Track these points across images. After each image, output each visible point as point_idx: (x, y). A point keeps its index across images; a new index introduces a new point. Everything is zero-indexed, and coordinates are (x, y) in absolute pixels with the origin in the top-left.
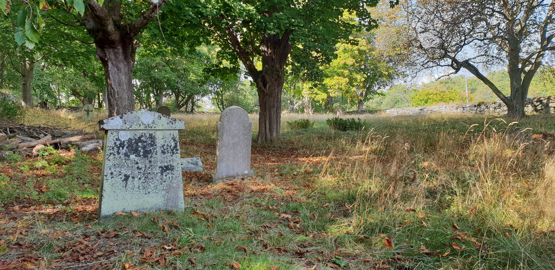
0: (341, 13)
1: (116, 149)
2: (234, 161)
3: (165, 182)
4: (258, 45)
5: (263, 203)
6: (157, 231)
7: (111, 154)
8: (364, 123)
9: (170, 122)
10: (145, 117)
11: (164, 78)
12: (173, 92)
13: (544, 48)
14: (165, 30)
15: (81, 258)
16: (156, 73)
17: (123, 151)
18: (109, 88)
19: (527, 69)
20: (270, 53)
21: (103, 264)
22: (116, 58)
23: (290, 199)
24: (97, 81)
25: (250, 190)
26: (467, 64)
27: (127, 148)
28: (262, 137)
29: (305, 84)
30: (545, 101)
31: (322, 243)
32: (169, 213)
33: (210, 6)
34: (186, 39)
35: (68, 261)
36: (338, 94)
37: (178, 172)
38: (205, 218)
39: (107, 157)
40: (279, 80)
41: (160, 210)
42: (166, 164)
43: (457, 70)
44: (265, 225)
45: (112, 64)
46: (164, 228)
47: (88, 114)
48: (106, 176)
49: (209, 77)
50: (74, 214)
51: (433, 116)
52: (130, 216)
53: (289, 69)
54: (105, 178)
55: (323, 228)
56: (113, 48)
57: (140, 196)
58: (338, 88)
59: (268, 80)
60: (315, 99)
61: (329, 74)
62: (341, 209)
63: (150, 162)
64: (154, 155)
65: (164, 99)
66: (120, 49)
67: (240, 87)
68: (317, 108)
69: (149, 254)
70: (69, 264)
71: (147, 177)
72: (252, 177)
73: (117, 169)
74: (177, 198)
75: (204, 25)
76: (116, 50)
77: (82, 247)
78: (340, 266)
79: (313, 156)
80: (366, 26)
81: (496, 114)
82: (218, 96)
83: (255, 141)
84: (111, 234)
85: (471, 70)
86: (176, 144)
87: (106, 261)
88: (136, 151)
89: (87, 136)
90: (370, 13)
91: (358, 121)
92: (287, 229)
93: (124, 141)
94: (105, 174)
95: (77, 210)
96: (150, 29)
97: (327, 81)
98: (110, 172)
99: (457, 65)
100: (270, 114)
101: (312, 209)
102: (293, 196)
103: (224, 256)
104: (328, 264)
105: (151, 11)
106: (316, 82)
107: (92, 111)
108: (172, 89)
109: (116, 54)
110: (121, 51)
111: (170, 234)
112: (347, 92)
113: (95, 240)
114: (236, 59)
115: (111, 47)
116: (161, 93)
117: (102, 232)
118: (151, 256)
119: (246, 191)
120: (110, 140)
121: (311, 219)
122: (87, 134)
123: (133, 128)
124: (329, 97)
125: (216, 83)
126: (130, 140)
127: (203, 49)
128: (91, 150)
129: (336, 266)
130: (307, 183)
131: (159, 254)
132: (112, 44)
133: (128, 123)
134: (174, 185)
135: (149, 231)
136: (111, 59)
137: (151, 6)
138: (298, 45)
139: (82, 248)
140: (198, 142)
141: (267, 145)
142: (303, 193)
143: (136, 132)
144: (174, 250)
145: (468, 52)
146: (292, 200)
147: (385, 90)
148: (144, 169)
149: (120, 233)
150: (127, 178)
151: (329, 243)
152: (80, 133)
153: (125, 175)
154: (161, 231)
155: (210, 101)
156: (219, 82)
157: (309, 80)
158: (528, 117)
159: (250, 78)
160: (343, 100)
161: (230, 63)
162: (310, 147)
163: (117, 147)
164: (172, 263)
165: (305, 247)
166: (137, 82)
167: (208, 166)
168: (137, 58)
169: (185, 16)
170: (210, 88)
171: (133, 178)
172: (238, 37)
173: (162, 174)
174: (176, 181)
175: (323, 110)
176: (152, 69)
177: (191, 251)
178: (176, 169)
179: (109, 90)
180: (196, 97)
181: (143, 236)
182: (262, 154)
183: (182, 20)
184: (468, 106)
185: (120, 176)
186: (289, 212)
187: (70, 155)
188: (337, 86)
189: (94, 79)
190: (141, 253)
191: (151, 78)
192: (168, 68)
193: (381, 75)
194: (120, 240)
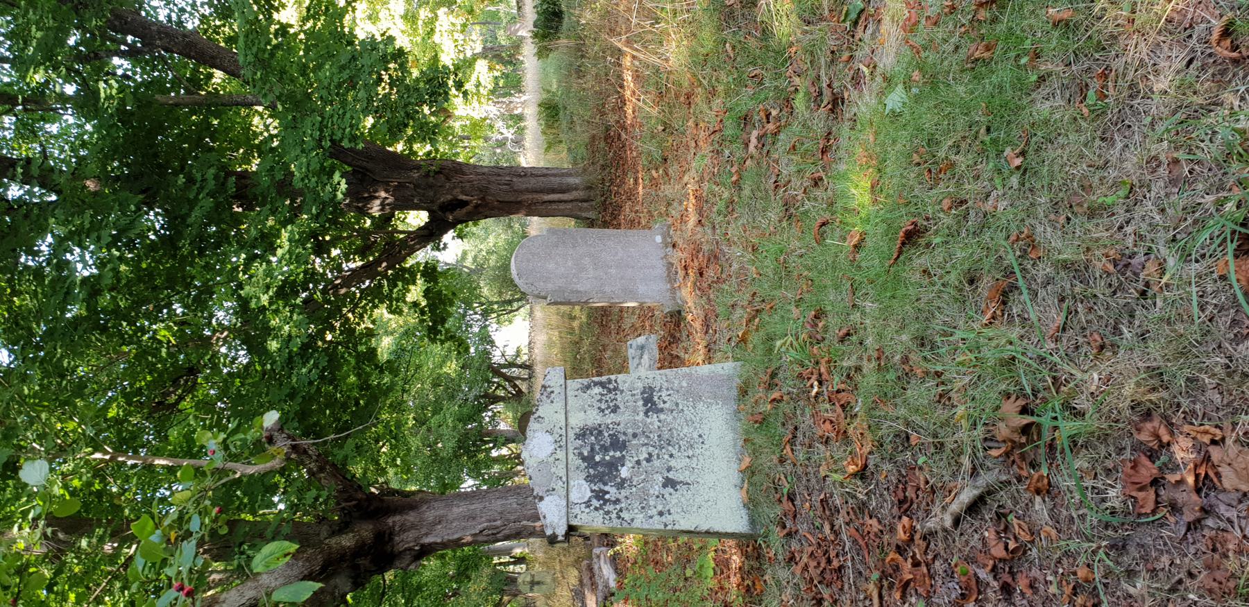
0: (283, 29)
1: (608, 507)
2: (633, 266)
3: (677, 404)
4: (369, 222)
5: (726, 195)
6: (781, 414)
10: (539, 447)
11: (455, 428)
12: (486, 409)
14: (346, 427)
15: (835, 564)
16: (445, 446)
17: (612, 492)
18: (480, 538)
20: (387, 191)
21: (847, 520)
22: (413, 526)
23: (718, 135)
24: (467, 569)
25: (699, 229)
27: (605, 484)
28: (580, 209)
29: (457, 113)
31: (812, 53)
32: (743, 392)
33: (287, 328)
34: (366, 381)
35: (842, 589)
36: (476, 33)
37: (659, 378)
38: (754, 317)
40: (450, 170)
41: (738, 412)
42: (641, 403)
44: (773, 186)
45: (427, 535)
46: (774, 400)
47: (538, 583)
48: (666, 525)
49: (447, 331)
50: (748, 591)
52: (750, 473)
53: (421, 149)
54: (669, 527)
55: (781, 56)
57: (708, 453)
58: (462, 32)
59: (449, 197)
60: (490, 87)
61: (428, 56)
62: (738, 13)
63: (635, 435)
65: (503, 426)
66: (394, 520)
67: (469, 262)
68: (510, 85)
69: (828, 426)
70: (846, 587)
72: (669, 227)
73: (652, 503)
75: (331, 342)
76: (397, 528)
77: (813, 564)
78: (862, 11)
79: (622, 87)
82: (493, 311)
83: (591, 224)
84: (787, 508)
86: (596, 384)
87: (843, 512)
88: (614, 466)
89: (586, 580)
92: (782, 136)
93: (592, 491)
94: (662, 527)
95: (738, 586)
96: (346, 457)
97: (447, 58)
98: (657, 518)
100: (528, 191)
101: (740, 82)
102: (712, 130)
103: (834, 268)
104: (857, 37)
105: (303, 457)
106: (451, 83)
107: (533, 576)
108: (480, 411)
109: (404, 529)
110: (397, 518)
111: (787, 386)
112: (471, 12)
113: (800, 541)
114: (404, 270)
115: (391, 539)
116: (489, 434)
117: (784, 527)
118: (832, 422)
119: (699, 236)
120: (592, 521)
121: (761, 83)
122: (581, 581)
123: (562, 473)
124: (483, 55)
125: (464, 316)
126: (589, 479)
127: (385, 346)
128: (616, 570)
129: (863, 18)
130: (682, 99)
131: (828, 406)
133: (553, 485)
134: (684, 384)
135: (781, 429)
136: (416, 539)
137: (293, 456)
138: (364, 127)
139: (815, 564)
140: (596, 340)
141: (596, 195)
142: (705, 107)
143: (571, 467)
144: (820, 375)
146: (720, 130)
148: (651, 449)
149: (785, 491)
150: (669, 483)
151: (811, 37)
153: (665, 486)
154: (781, 405)
155: (504, 328)
156: (461, 311)
157: (447, 100)
159: (448, 237)
160: (491, 21)
161: (414, 283)
162: (602, 96)
163: (605, 504)
164: (848, 376)
165: (820, 94)
166: (468, 484)
167: (647, 324)
168: (413, 488)
169: (311, 383)
170: (476, 330)
171: (669, 469)
172: (352, 265)
173: (662, 410)
174: (676, 382)
175: (514, 71)
176: (437, 454)
177: (824, 339)
180: (497, 358)
181: (792, 441)
182: (620, 207)
183: (319, 389)
186: (745, 136)
188: (456, 35)
189: (463, 574)
190: (827, 442)
191: (456, 457)
192: (433, 422)
194: (801, 490)
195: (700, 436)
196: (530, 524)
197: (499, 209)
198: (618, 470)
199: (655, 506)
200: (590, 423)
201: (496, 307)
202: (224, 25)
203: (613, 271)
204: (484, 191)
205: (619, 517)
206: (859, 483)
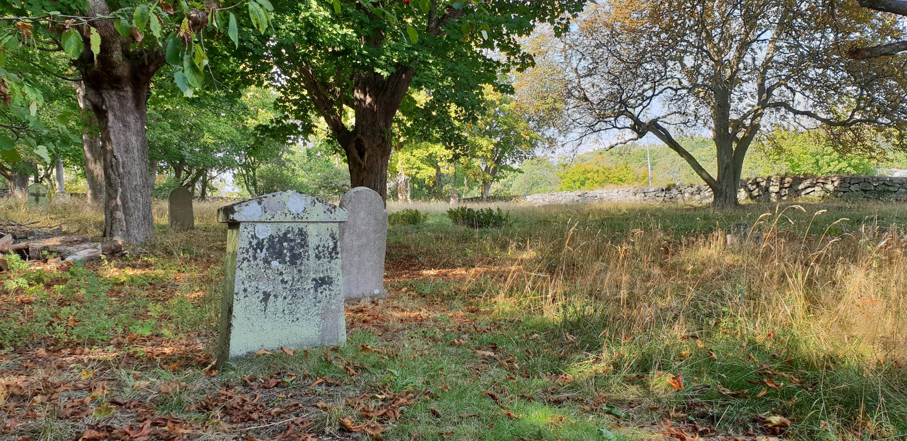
3: (320, 302)
7: (244, 259)
8: (507, 215)
9: (328, 210)
11: (160, 139)
13: (763, 104)
17: (261, 255)
18: (109, 156)
19: (740, 135)
26: (654, 126)
29: (400, 153)
30: (764, 184)
40: (384, 149)
42: (322, 276)
43: (641, 135)
45: (115, 115)
47: (37, 200)
48: (237, 294)
51: (605, 206)
54: (235, 296)
56: (118, 89)
63: (300, 271)
64: (305, 261)
66: (129, 91)
73: (253, 283)
76: (122, 93)
80: (517, 64)
81: (695, 204)
85: (660, 136)
86: (335, 243)
88: (280, 256)
89: (69, 239)
90: (519, 46)
93: (263, 240)
98: (242, 287)
99: (640, 129)
110: (130, 94)
114: (306, 111)
115: (113, 88)
123: (276, 219)
124: (439, 175)
126: (271, 238)
132: (115, 83)
136: (112, 108)
143: (280, 225)
145: (656, 109)
147: (526, 166)
150: (267, 296)
152: (59, 232)
153: (264, 293)
158: (743, 207)
163: (254, 249)
171: (276, 296)
173: (316, 291)
178: (336, 282)
179: (108, 160)
184: (651, 190)
185: (257, 295)
187: (52, 266)
195: (298, 319)
196: (119, 194)
198: (276, 259)
199: (251, 286)
203: (356, 259)
205: (244, 259)
206: (337, 428)
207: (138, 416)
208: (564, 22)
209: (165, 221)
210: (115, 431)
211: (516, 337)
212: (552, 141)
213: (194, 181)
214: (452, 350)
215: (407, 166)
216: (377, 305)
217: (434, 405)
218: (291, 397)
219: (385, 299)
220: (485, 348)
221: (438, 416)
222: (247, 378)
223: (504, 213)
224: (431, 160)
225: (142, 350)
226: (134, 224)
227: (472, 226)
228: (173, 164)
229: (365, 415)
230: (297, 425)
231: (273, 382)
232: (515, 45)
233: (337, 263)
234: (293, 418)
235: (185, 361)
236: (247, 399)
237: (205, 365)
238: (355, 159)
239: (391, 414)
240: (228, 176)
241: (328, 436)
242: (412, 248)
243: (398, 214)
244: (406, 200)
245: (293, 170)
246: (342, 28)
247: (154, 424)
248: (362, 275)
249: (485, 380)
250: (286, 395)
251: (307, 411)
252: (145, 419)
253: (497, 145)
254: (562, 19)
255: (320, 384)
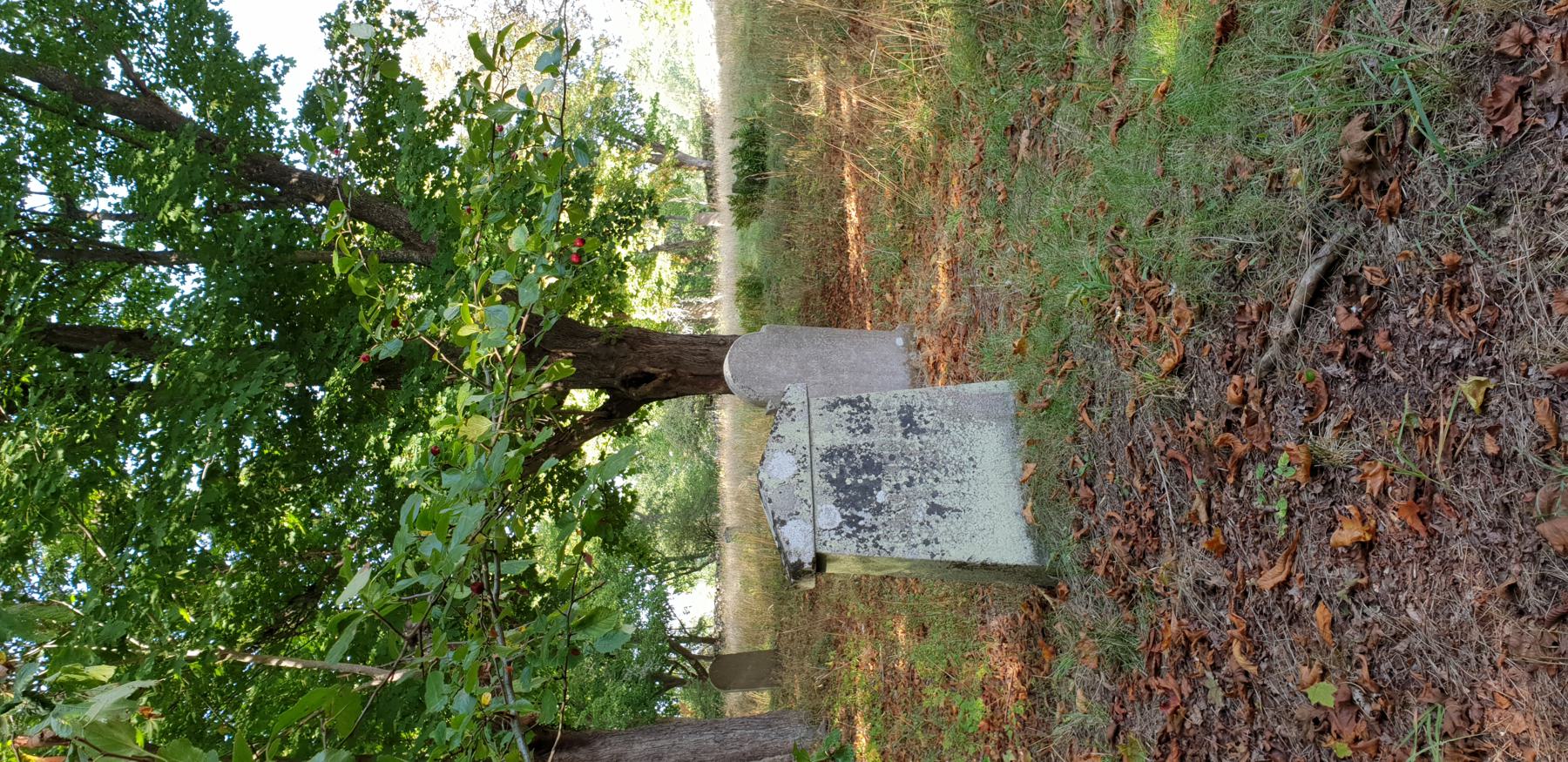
3: (942, 425)
7: (876, 546)
9: (788, 415)
17: (867, 518)
27: (859, 509)
39: (883, 553)
42: (898, 423)
48: (933, 555)
54: (937, 558)
59: (634, 369)
60: (673, 285)
63: (892, 458)
64: (875, 449)
71: (931, 464)
73: (915, 530)
74: (982, 396)
86: (844, 402)
88: (868, 490)
91: (737, 140)
98: (921, 547)
114: (572, 474)
123: (808, 496)
124: (668, 247)
126: (839, 503)
133: (797, 508)
143: (818, 491)
147: (645, 89)
148: (912, 472)
150: (934, 509)
153: (930, 512)
171: (935, 495)
173: (923, 431)
185: (933, 523)
193: (604, 103)
197: (693, 384)
200: (838, 444)
201: (673, 564)
202: (370, 183)
204: (674, 362)
205: (876, 546)
206: (1177, 379)
207: (1140, 699)
208: (398, 18)
209: (763, 698)
210: (1170, 729)
211: (993, 91)
212: (602, 43)
213: (687, 655)
214: (1018, 201)
215: (656, 304)
216: (923, 340)
217: (1138, 223)
218: (1113, 460)
219: (912, 328)
220: (1013, 146)
221: (1160, 214)
222: (1076, 534)
223: (738, 127)
224: (645, 262)
225: (1014, 708)
226: (779, 742)
227: (764, 183)
228: (661, 691)
229: (1155, 338)
230: (1167, 447)
231: (1084, 492)
232: (441, 109)
233: (877, 398)
234: (1155, 453)
235: (1036, 640)
236: (1115, 530)
237: (1044, 606)
238: (656, 388)
239: (1153, 294)
240: (677, 602)
241: (1190, 395)
242: (809, 288)
243: (743, 317)
244: (713, 305)
245: (666, 495)
246: (436, 414)
247: (1157, 672)
248: (875, 360)
249: (1080, 141)
250: (1109, 468)
251: (1142, 432)
252: (1148, 687)
253: (611, 141)
254: (393, 24)
255: (1091, 415)
